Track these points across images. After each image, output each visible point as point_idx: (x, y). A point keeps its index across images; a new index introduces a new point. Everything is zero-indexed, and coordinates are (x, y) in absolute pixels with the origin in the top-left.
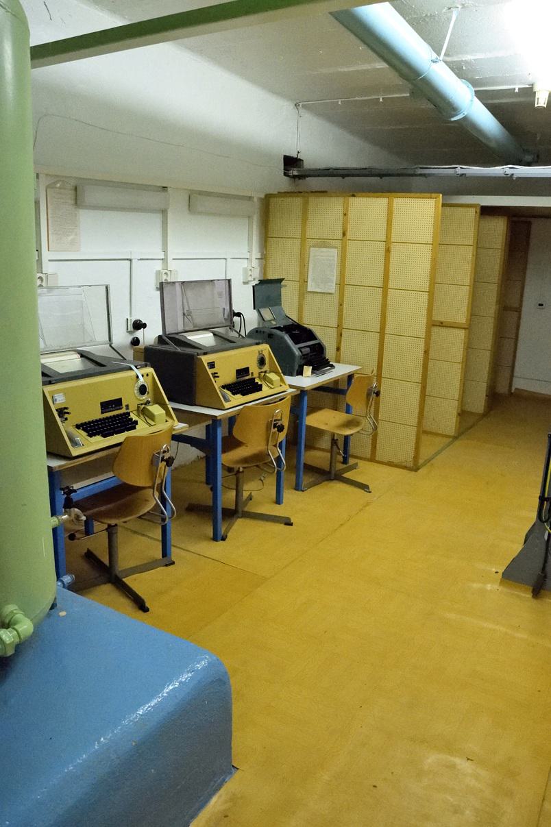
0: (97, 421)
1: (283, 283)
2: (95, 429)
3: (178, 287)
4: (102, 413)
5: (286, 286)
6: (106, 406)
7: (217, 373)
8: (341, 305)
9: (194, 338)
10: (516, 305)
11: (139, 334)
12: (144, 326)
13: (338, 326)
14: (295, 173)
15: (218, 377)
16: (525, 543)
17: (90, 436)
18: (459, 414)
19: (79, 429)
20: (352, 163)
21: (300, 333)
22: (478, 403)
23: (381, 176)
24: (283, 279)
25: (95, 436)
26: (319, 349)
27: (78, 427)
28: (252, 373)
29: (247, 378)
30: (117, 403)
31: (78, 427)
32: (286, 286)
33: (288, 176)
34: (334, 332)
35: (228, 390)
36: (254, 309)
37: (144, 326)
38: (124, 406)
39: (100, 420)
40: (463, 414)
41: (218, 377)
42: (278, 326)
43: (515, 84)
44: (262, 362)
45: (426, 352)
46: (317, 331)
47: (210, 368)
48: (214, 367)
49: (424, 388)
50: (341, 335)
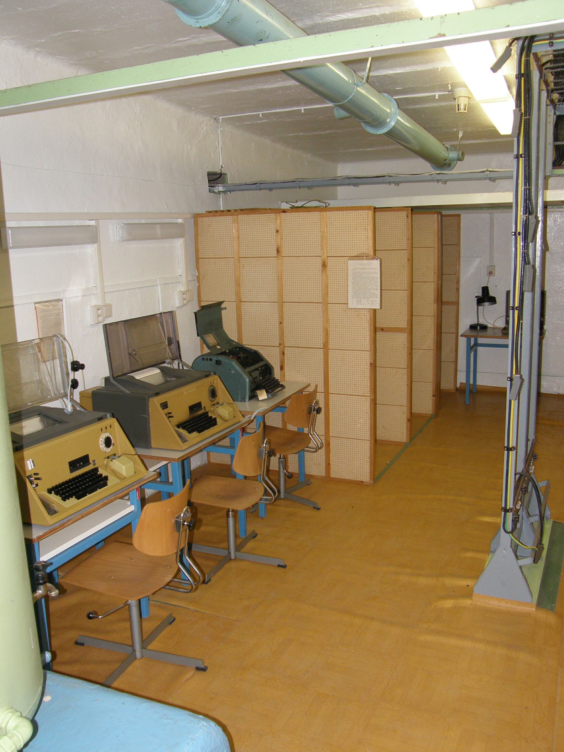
0: (67, 482)
1: (223, 306)
2: (67, 492)
3: (121, 328)
4: (71, 472)
5: (225, 308)
6: (74, 465)
7: (171, 413)
8: (281, 323)
9: (139, 376)
10: (454, 300)
11: (78, 375)
12: (82, 367)
13: (280, 344)
14: (221, 189)
15: (172, 417)
16: (178, 342)
17: (64, 499)
18: (409, 420)
19: (51, 493)
20: (279, 176)
21: (249, 358)
22: (426, 404)
23: (309, 187)
24: (221, 303)
25: (69, 499)
26: (267, 369)
27: (50, 491)
28: (204, 407)
29: (200, 412)
30: (85, 460)
31: (50, 491)
32: (225, 308)
33: (214, 192)
34: (277, 351)
35: (183, 428)
36: (198, 335)
37: (82, 367)
38: (91, 461)
39: (70, 481)
40: (413, 418)
41: (172, 417)
42: (223, 350)
43: (435, 91)
44: (213, 393)
45: (374, 366)
46: (264, 352)
47: (163, 409)
48: (167, 407)
49: (374, 402)
50: (283, 353)
